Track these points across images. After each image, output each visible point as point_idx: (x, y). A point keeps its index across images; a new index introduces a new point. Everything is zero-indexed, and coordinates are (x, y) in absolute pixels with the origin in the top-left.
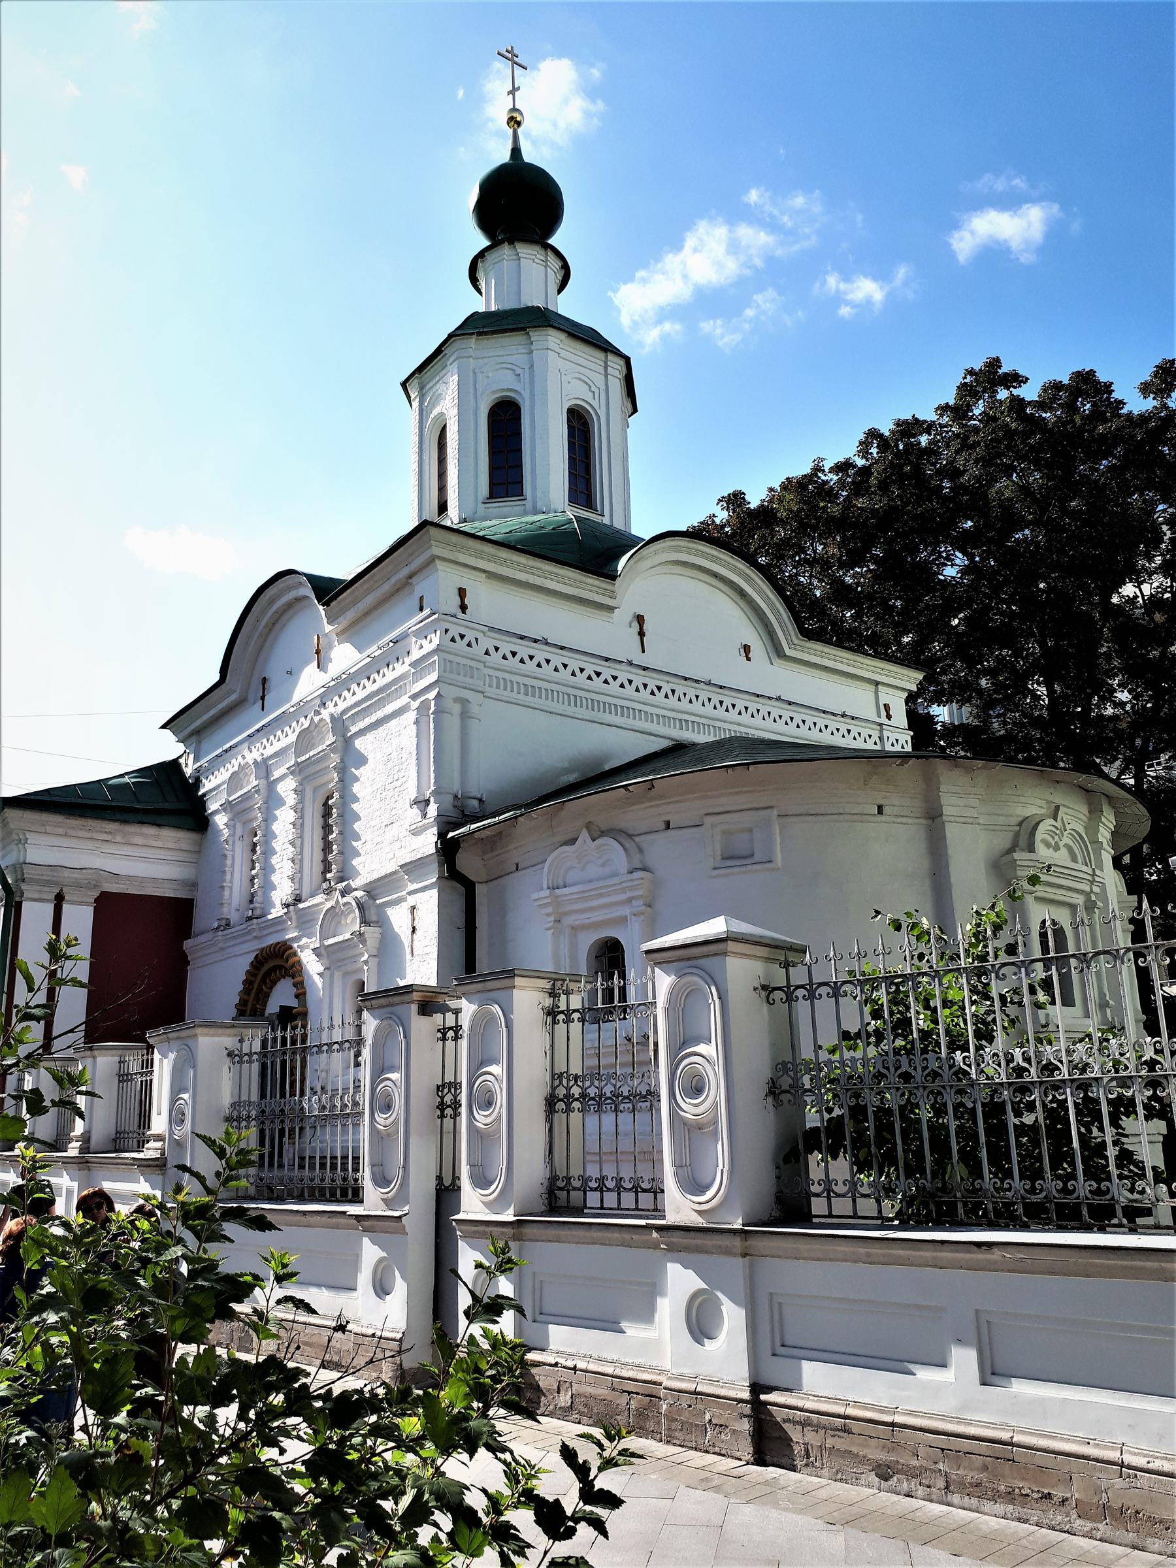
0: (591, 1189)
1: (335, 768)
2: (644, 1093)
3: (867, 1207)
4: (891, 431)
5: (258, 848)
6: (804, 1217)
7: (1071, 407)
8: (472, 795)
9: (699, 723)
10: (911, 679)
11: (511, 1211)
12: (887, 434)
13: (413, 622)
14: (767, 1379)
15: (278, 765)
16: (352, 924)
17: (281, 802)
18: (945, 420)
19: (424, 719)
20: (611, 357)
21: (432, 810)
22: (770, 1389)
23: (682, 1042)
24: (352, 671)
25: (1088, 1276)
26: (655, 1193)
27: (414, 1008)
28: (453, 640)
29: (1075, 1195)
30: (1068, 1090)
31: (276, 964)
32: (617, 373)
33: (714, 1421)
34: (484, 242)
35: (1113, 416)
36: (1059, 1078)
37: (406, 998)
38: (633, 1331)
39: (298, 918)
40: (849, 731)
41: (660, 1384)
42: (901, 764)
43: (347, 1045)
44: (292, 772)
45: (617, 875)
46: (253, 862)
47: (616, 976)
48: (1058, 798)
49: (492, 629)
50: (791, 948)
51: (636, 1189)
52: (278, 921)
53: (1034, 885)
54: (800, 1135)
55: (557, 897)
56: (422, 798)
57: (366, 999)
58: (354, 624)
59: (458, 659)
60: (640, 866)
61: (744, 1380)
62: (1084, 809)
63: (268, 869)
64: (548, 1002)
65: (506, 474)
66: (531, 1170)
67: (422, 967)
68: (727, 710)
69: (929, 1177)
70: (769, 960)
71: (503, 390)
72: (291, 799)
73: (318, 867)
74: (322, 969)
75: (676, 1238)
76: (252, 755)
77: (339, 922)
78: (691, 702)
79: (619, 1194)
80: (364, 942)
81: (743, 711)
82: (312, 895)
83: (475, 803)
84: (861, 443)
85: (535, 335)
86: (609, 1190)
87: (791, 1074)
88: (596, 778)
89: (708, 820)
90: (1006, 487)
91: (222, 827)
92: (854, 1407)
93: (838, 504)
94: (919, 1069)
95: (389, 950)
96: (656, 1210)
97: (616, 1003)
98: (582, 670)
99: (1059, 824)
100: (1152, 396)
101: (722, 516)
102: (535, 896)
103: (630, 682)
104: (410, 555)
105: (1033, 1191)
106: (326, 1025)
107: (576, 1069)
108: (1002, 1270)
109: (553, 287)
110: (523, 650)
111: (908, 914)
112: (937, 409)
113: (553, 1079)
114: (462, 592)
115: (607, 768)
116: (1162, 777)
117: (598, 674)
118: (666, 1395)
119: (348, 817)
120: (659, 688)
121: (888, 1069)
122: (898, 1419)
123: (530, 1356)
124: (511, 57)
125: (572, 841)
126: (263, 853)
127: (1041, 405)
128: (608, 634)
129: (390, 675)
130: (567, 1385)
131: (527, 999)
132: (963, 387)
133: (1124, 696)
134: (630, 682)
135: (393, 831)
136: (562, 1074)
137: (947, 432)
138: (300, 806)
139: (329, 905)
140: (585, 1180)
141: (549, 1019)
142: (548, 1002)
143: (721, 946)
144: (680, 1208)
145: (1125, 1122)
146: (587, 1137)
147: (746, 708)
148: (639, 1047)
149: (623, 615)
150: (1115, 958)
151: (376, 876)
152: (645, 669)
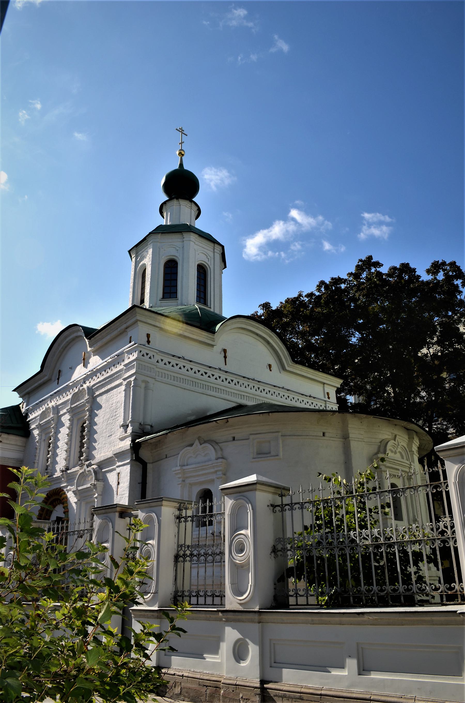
0: (193, 596)
1: (87, 410)
2: (218, 553)
3: (312, 600)
4: (330, 282)
5: (52, 445)
6: (287, 606)
7: (400, 277)
8: (147, 423)
9: (249, 397)
10: (338, 382)
11: (157, 605)
12: (328, 283)
13: (126, 348)
14: (267, 678)
15: (62, 409)
16: (92, 480)
17: (63, 425)
18: (351, 278)
19: (128, 389)
20: (216, 245)
21: (130, 429)
22: (268, 682)
23: (235, 528)
24: (98, 368)
25: (403, 625)
26: (221, 597)
27: (117, 514)
28: (143, 355)
29: (398, 592)
30: (396, 547)
31: (56, 497)
32: (218, 252)
33: (244, 697)
34: (166, 198)
35: (416, 281)
36: (393, 541)
37: (114, 510)
38: (210, 658)
39: (67, 477)
40: (312, 403)
41: (220, 682)
42: (333, 415)
43: (86, 531)
44: (68, 411)
45: (211, 461)
46: (49, 451)
47: (208, 501)
48: (396, 432)
49: (160, 352)
50: (284, 488)
51: (213, 596)
52: (58, 478)
53: (383, 462)
54: (285, 570)
55: (184, 470)
56: (125, 424)
57: (97, 511)
58: (101, 347)
59: (147, 364)
60: (221, 457)
61: (257, 678)
62: (406, 437)
63: (55, 455)
64: (177, 513)
65: (170, 288)
66: (167, 587)
67: (122, 497)
68: (261, 392)
69: (339, 586)
70: (274, 493)
71: (171, 256)
72: (67, 424)
73: (77, 454)
74: (76, 500)
75: (230, 616)
76: (52, 404)
77: (85, 479)
78: (246, 387)
79: (205, 598)
80: (96, 488)
81: (268, 392)
82: (74, 467)
83: (149, 427)
84: (318, 286)
85: (186, 235)
86: (201, 596)
87: (282, 543)
88: (204, 418)
89: (251, 437)
90: (376, 307)
91: (36, 436)
92: (305, 688)
93: (308, 310)
94: (336, 539)
95: (107, 490)
96: (221, 605)
97: (207, 513)
98: (199, 371)
99: (396, 443)
100: (431, 274)
101: (261, 312)
102: (174, 469)
103: (220, 377)
104: (127, 319)
105: (382, 591)
106: (77, 522)
107: (188, 543)
108: (368, 625)
109: (194, 217)
110: (174, 361)
111: (333, 475)
112: (348, 274)
113: (178, 547)
114: (148, 336)
115: (208, 414)
116: (439, 428)
117: (206, 373)
118: (223, 686)
119: (92, 432)
120: (232, 381)
121: (323, 539)
122: (323, 692)
123: (163, 671)
124: (181, 131)
125: (191, 445)
126: (53, 448)
127: (388, 275)
128: (212, 357)
129: (115, 370)
130: (179, 683)
131: (168, 511)
132: (358, 266)
133: (423, 394)
134: (220, 377)
135: (112, 438)
136: (182, 545)
137: (352, 284)
138: (71, 427)
139: (81, 471)
140: (190, 592)
141: (177, 521)
142: (177, 513)
143: (254, 486)
144: (232, 602)
145: (420, 564)
146: (192, 578)
147: (269, 391)
148: (218, 538)
149: (218, 348)
150: (414, 490)
151: (102, 459)
152: (226, 372)
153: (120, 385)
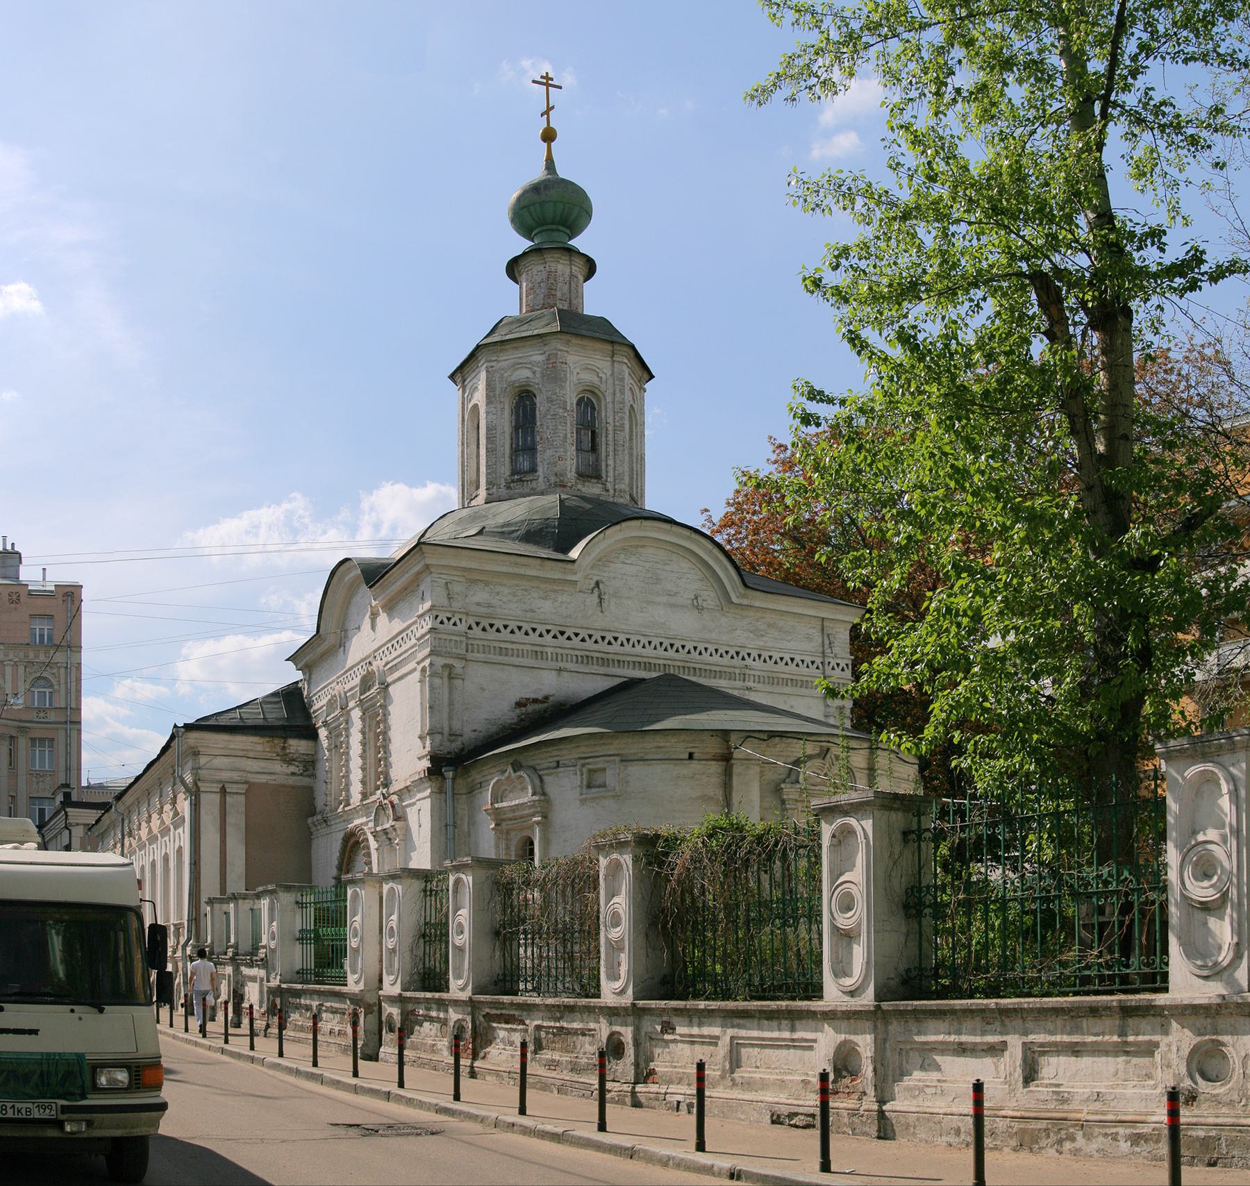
135: (409, 757)
153: (415, 670)
